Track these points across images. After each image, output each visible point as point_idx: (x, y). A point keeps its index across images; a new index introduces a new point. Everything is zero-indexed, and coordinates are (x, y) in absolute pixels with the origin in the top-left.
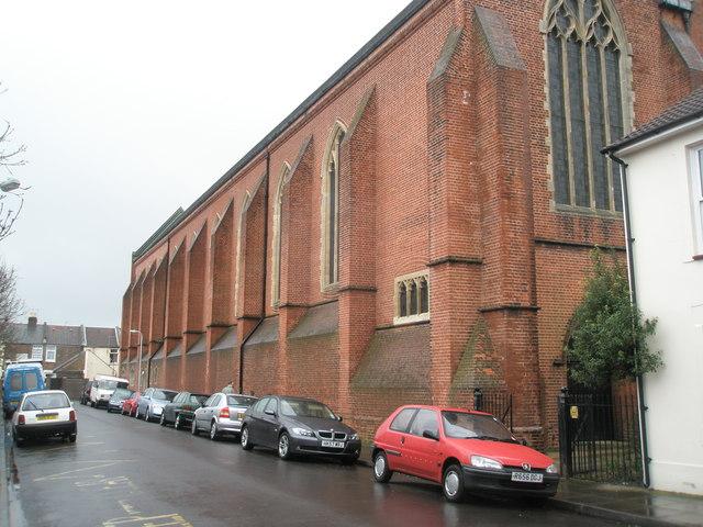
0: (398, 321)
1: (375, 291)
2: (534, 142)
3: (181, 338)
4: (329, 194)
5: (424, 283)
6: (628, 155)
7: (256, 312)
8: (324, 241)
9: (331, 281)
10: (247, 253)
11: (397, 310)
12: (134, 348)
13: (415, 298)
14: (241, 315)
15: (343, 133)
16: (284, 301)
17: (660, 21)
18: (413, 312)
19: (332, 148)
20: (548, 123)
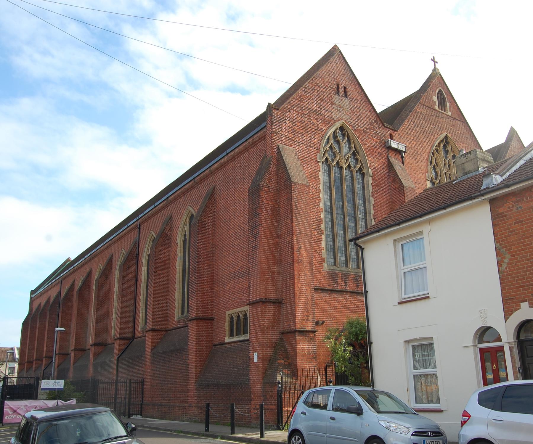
0: (227, 340)
1: (212, 319)
2: (314, 227)
3: (68, 354)
4: (182, 254)
5: (245, 315)
6: (364, 242)
7: (129, 335)
8: (178, 286)
9: (183, 313)
10: (122, 293)
11: (227, 333)
12: (30, 363)
13: (240, 325)
14: (117, 336)
15: (192, 215)
16: (149, 326)
17: (387, 157)
18: (238, 334)
19: (185, 224)
20: (322, 216)
